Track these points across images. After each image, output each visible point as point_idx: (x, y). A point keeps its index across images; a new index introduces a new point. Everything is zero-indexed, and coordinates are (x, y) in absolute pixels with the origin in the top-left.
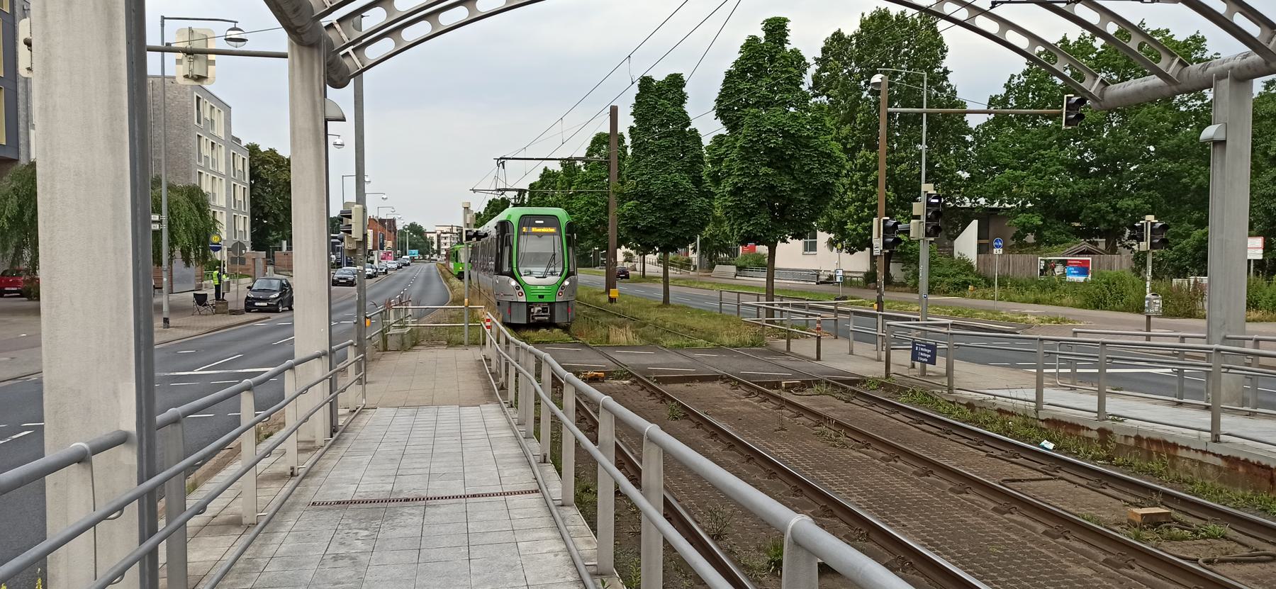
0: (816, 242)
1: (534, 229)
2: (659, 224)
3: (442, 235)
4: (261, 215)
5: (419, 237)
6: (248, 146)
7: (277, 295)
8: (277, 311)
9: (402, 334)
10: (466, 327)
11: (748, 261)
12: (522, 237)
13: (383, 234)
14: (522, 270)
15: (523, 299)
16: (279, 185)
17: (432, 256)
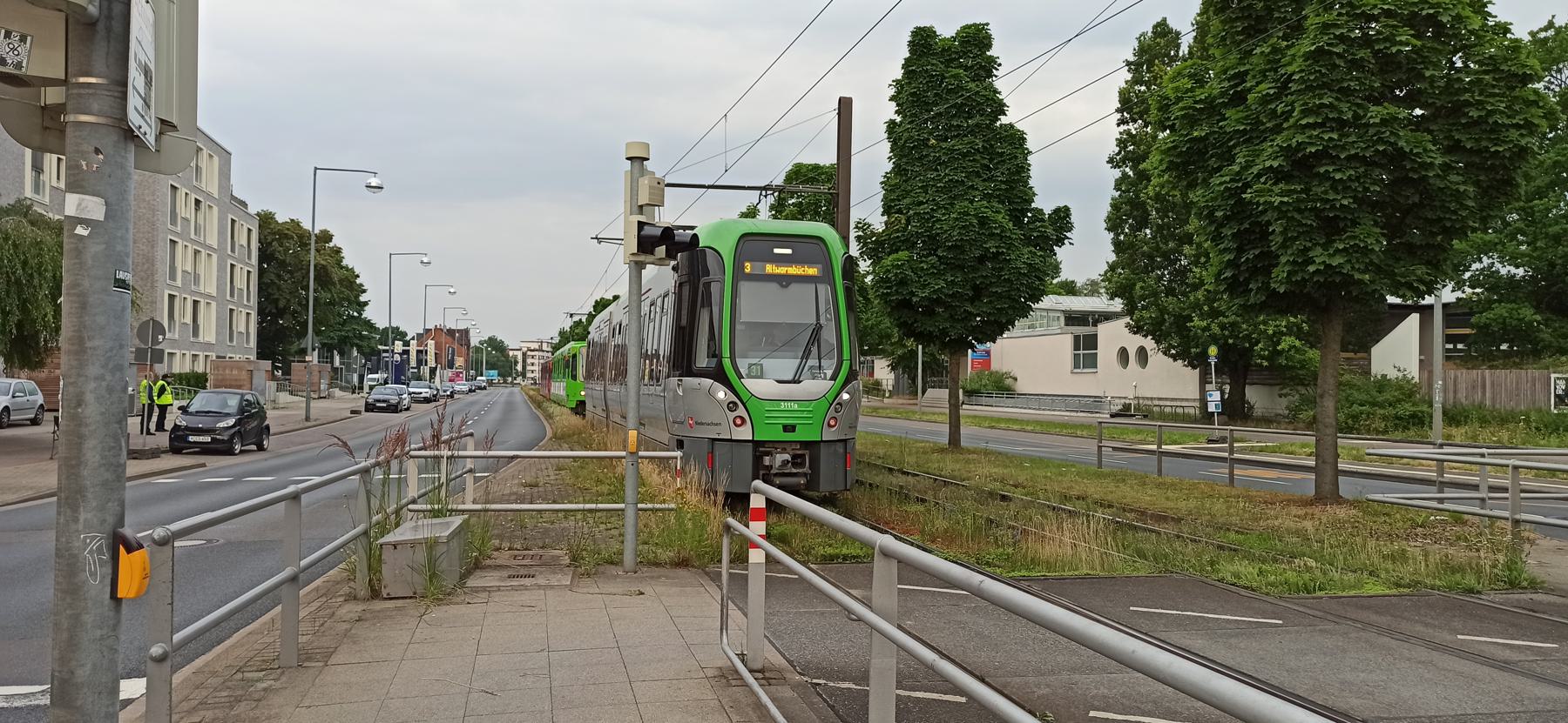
0: (1096, 354)
1: (770, 268)
2: (953, 296)
3: (529, 353)
4: (274, 311)
5: (499, 354)
6: (258, 214)
7: (231, 422)
8: (230, 452)
9: (432, 544)
10: (630, 513)
11: (983, 383)
12: (744, 287)
14: (743, 365)
15: (744, 433)
16: (302, 269)
17: (515, 379)
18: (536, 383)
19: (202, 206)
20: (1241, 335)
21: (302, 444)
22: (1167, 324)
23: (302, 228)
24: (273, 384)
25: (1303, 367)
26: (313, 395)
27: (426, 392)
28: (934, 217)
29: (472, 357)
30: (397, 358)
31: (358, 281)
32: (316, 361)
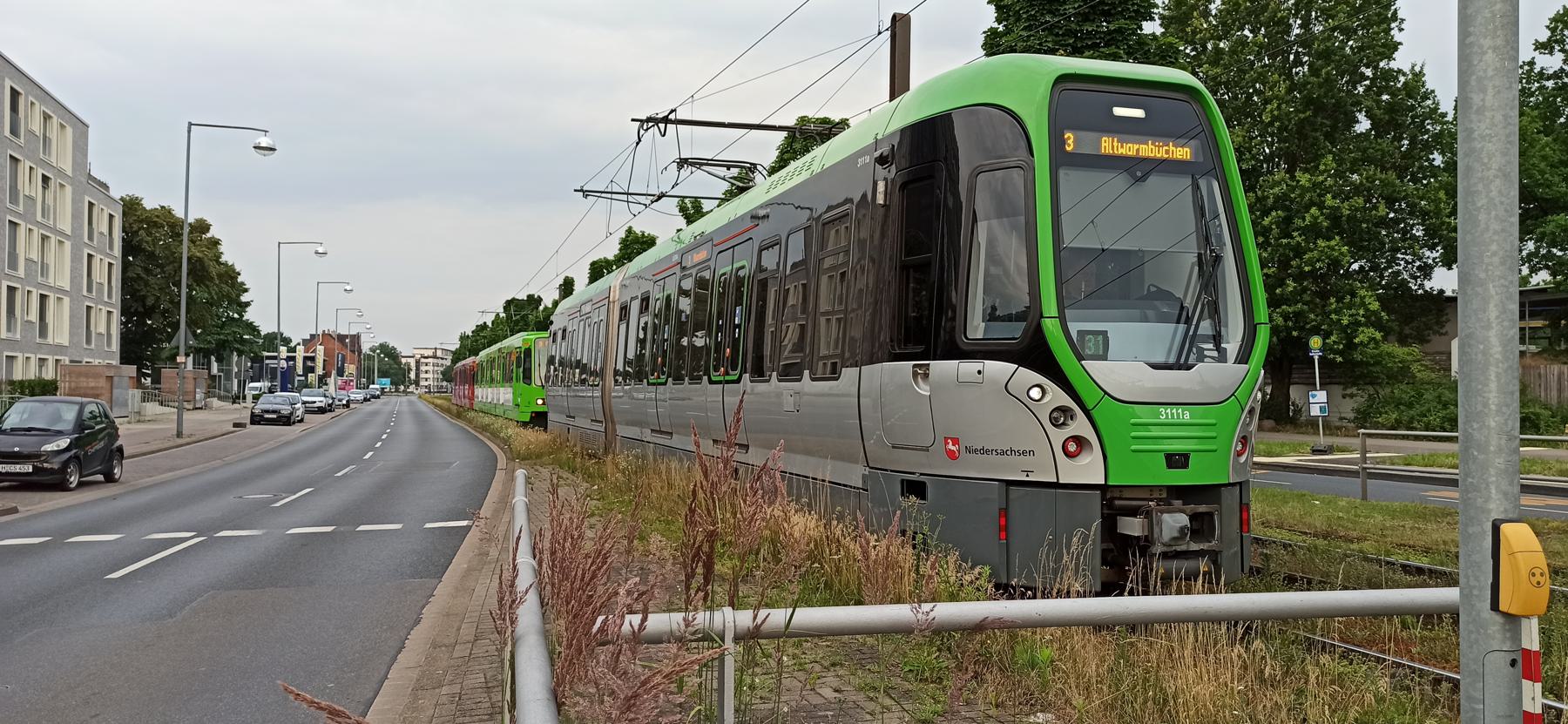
1: (1109, 145)
3: (423, 360)
5: (392, 362)
7: (64, 443)
8: (61, 486)
13: (343, 355)
15: (1088, 470)
18: (430, 392)
19: (52, 184)
20: (1308, 326)
23: (174, 216)
24: (138, 393)
25: (1377, 363)
26: (186, 405)
27: (320, 401)
30: (284, 364)
32: (190, 366)
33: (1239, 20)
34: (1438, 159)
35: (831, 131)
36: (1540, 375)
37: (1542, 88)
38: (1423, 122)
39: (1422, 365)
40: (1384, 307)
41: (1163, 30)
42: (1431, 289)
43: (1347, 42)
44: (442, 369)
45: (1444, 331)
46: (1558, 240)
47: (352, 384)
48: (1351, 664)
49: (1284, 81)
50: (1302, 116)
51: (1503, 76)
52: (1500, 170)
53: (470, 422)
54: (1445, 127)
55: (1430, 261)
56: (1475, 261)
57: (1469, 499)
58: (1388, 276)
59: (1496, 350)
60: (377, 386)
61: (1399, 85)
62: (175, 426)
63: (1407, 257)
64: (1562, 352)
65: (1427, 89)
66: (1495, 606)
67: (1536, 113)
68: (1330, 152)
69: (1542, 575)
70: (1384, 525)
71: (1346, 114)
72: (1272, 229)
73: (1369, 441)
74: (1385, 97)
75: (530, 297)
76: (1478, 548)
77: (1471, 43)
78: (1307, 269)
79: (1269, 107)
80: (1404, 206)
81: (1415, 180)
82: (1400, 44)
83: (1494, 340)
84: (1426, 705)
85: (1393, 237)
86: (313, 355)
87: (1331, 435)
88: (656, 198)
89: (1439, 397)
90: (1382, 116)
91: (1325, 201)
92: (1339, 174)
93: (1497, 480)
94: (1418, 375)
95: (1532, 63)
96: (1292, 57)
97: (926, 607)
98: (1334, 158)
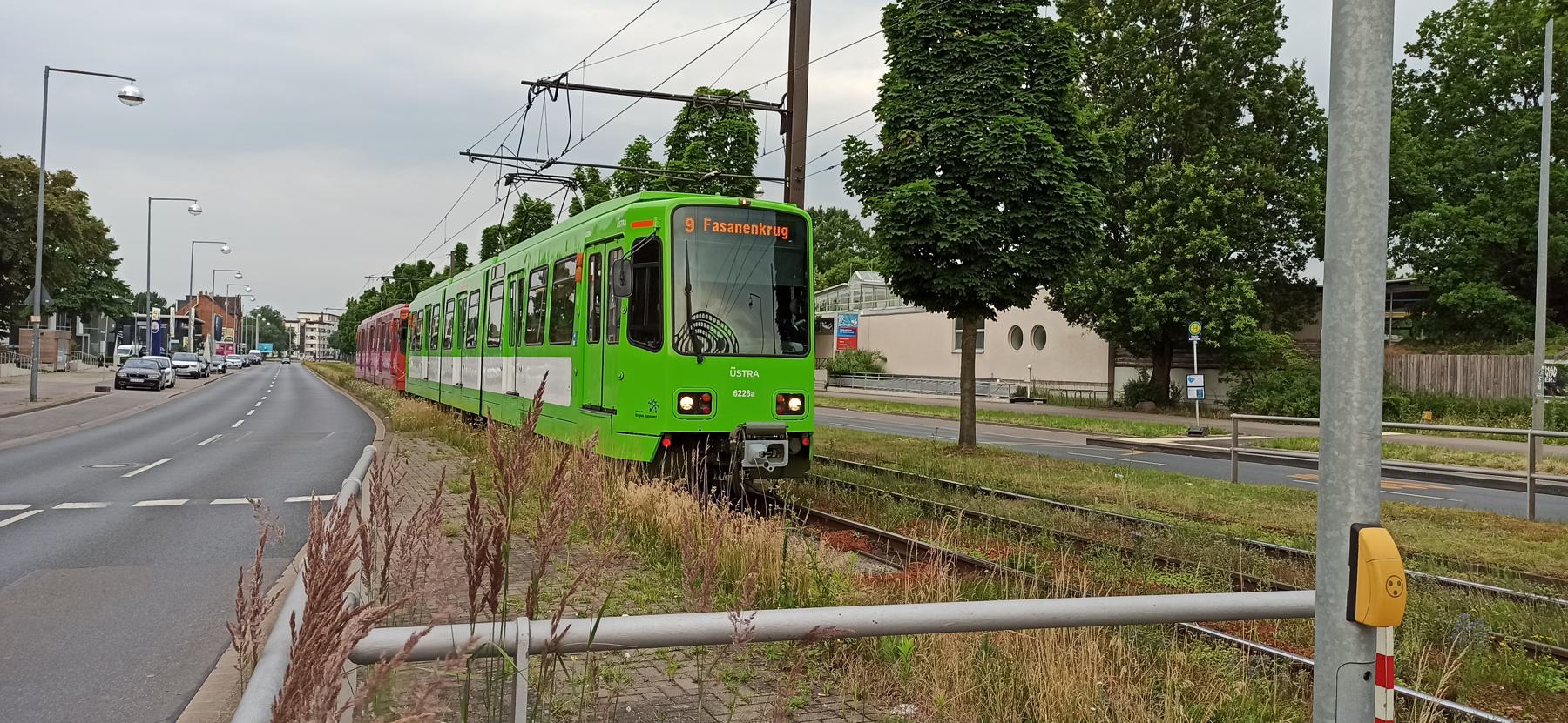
3: (308, 326)
5: (274, 326)
20: (1188, 312)
21: (19, 436)
22: (1104, 299)
27: (193, 366)
28: (963, 133)
29: (244, 328)
30: (156, 326)
31: (108, 236)
33: (1132, 10)
34: (1314, 154)
35: (727, 102)
36: (1401, 363)
37: (1412, 89)
38: (1302, 117)
39: (1293, 352)
40: (1260, 295)
41: (1060, 18)
42: (1304, 279)
43: (1233, 37)
44: (328, 335)
45: (1315, 320)
46: (1421, 235)
47: (230, 348)
48: (1214, 649)
49: (1173, 73)
50: (1189, 107)
51: (1377, 50)
52: (1370, 150)
53: (352, 390)
54: (1322, 123)
55: (1304, 252)
56: (1343, 248)
57: (1329, 501)
58: (1265, 266)
59: (1361, 343)
60: (258, 352)
61: (1281, 81)
62: (28, 388)
63: (1283, 248)
64: (1421, 342)
65: (1307, 86)
66: (1351, 616)
67: (1405, 113)
68: (1215, 144)
69: (1399, 584)
70: (1251, 507)
71: (1230, 107)
72: (1157, 217)
73: (1241, 424)
74: (1267, 92)
75: (422, 263)
76: (1336, 554)
77: (1346, 13)
78: (1189, 256)
79: (1159, 97)
80: (1281, 198)
81: (1292, 173)
82: (1283, 40)
83: (1359, 334)
84: (1284, 693)
85: (1270, 228)
86: (188, 317)
87: (1207, 417)
88: (545, 164)
89: (1308, 383)
90: (1264, 111)
91: (1208, 191)
92: (1223, 165)
93: (1357, 482)
94: (1289, 361)
95: (1403, 65)
96: (1181, 49)
97: (745, 615)
98: (1218, 151)
